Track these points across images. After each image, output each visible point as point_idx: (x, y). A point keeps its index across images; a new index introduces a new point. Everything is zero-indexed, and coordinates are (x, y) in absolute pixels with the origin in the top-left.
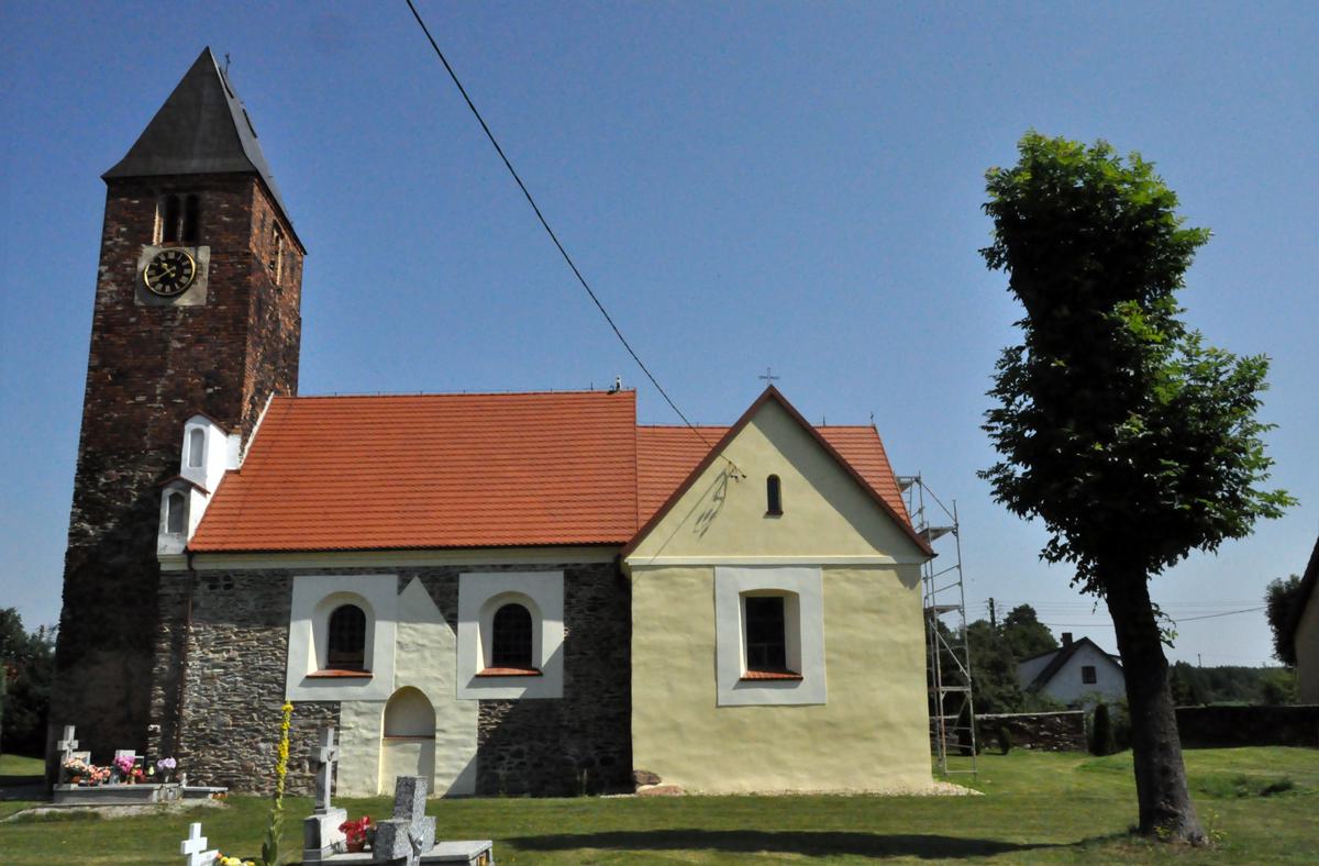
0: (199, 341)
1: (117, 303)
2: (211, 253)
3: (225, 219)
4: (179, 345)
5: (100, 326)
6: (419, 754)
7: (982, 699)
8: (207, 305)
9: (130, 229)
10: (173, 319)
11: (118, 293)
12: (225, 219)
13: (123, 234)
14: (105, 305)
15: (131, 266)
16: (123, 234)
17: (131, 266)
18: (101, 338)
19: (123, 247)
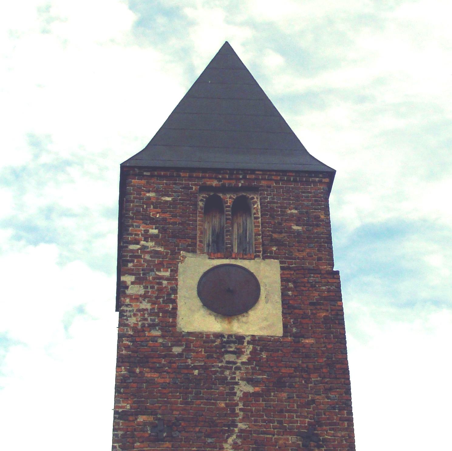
0: (280, 384)
1: (152, 326)
2: (282, 268)
3: (295, 227)
4: (250, 389)
5: (129, 357)
6: (208, 438)
7: (243, 354)
8: (285, 336)
9: (163, 230)
10: (239, 353)
11: (152, 313)
12: (295, 227)
13: (153, 237)
14: (134, 329)
15: (289, 289)
16: (153, 237)
17: (289, 289)
18: (131, 372)
19: (155, 254)
